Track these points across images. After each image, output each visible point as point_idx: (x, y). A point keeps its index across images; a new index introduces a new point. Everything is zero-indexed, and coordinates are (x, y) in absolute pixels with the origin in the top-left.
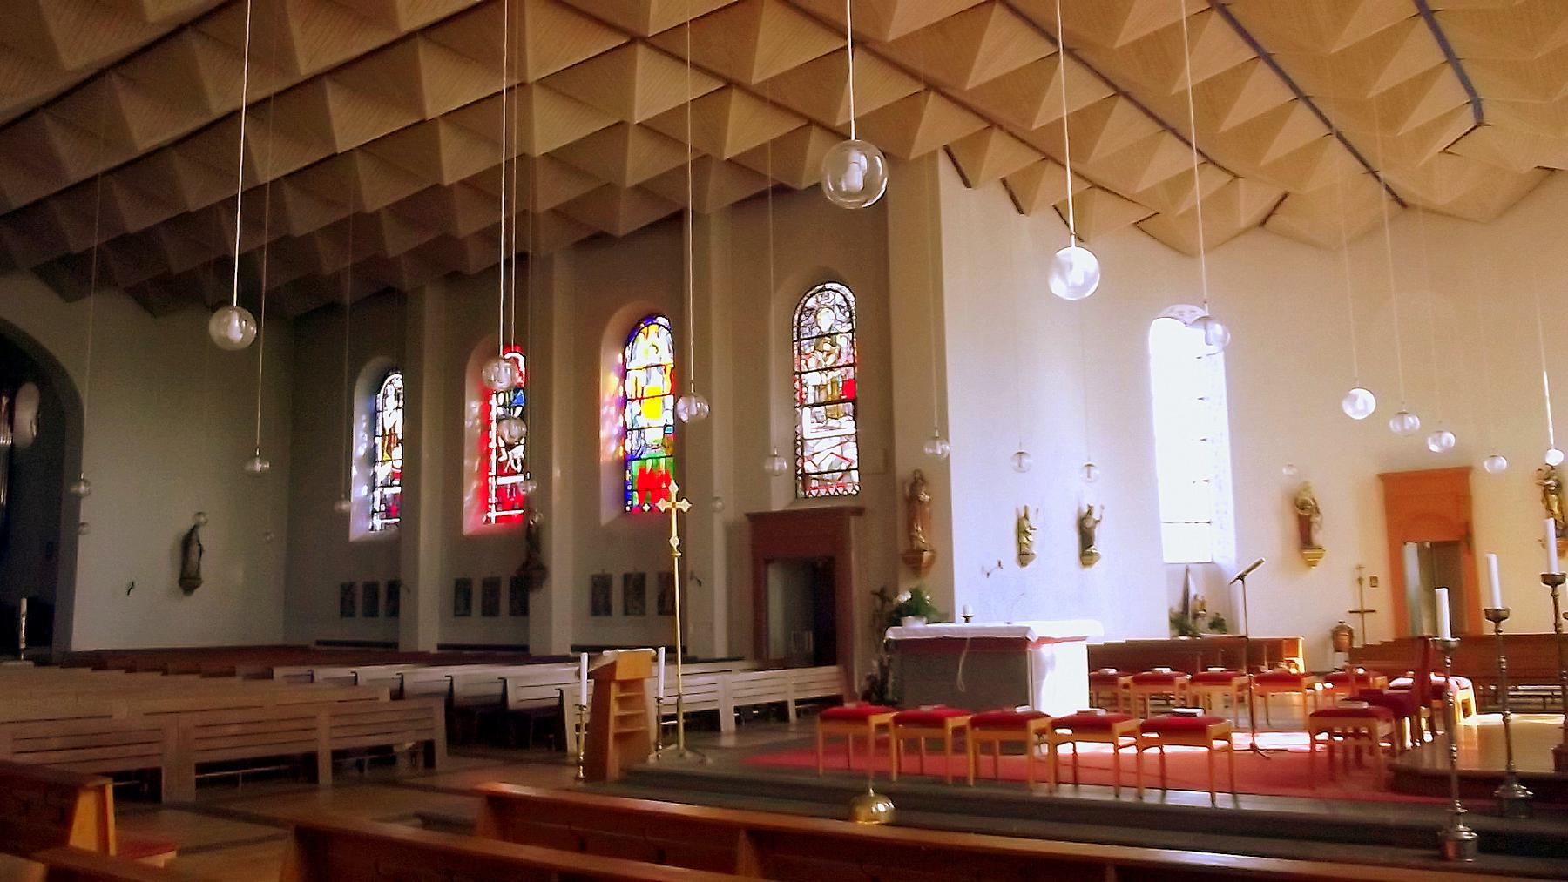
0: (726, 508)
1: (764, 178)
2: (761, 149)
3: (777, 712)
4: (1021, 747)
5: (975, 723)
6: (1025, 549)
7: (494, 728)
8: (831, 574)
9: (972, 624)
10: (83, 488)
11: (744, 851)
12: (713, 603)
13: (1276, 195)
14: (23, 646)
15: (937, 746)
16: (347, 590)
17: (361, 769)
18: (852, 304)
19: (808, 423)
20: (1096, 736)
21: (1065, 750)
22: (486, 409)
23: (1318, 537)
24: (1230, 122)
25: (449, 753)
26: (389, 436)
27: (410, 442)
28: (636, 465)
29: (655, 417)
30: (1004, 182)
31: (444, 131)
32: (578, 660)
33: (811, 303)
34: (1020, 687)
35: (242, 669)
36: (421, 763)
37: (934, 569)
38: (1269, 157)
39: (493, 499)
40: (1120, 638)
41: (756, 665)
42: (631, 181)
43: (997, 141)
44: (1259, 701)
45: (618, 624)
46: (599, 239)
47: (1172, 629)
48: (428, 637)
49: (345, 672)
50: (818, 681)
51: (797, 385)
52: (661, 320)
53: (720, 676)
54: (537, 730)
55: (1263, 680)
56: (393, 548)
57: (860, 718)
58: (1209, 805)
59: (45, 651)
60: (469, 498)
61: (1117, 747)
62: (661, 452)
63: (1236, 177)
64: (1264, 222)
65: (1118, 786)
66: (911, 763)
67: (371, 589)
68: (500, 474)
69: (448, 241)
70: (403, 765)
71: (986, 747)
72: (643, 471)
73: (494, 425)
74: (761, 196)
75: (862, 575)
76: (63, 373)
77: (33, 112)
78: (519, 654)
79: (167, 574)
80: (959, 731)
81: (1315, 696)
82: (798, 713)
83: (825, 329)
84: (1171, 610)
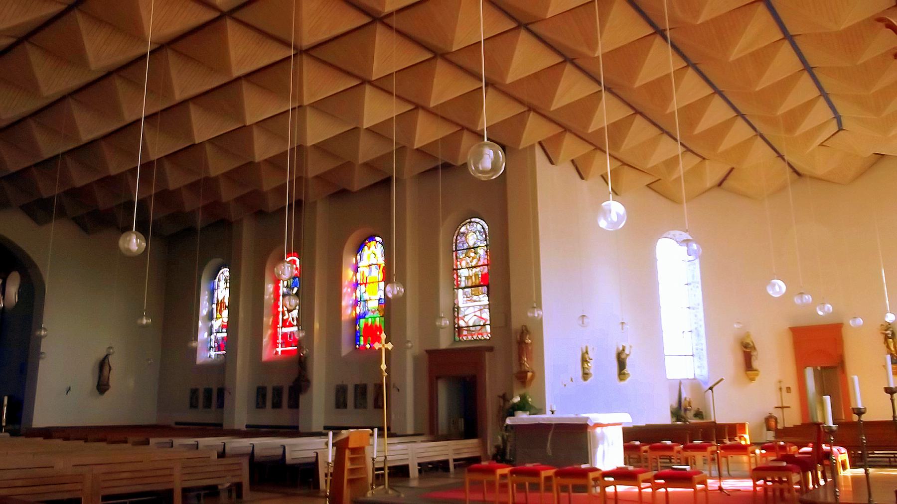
0: (414, 346)
1: (436, 159)
4: (584, 488)
5: (557, 474)
6: (586, 371)
8: (474, 387)
12: (407, 402)
14: (4, 424)
15: (535, 487)
16: (194, 392)
17: (199, 500)
18: (487, 231)
21: (610, 489)
22: (277, 288)
23: (755, 364)
26: (221, 304)
27: (233, 307)
30: (573, 161)
31: (256, 132)
33: (463, 229)
35: (131, 439)
36: (234, 495)
38: (722, 148)
39: (280, 341)
42: (360, 161)
45: (340, 418)
46: (342, 194)
49: (191, 441)
50: (466, 448)
51: (455, 276)
55: (726, 448)
56: (220, 368)
57: (491, 471)
60: (266, 339)
63: (704, 159)
64: (720, 185)
67: (208, 392)
68: (284, 325)
71: (564, 488)
72: (366, 325)
74: (435, 169)
78: (293, 431)
79: (89, 381)
80: (548, 479)
83: (471, 244)
84: (671, 406)
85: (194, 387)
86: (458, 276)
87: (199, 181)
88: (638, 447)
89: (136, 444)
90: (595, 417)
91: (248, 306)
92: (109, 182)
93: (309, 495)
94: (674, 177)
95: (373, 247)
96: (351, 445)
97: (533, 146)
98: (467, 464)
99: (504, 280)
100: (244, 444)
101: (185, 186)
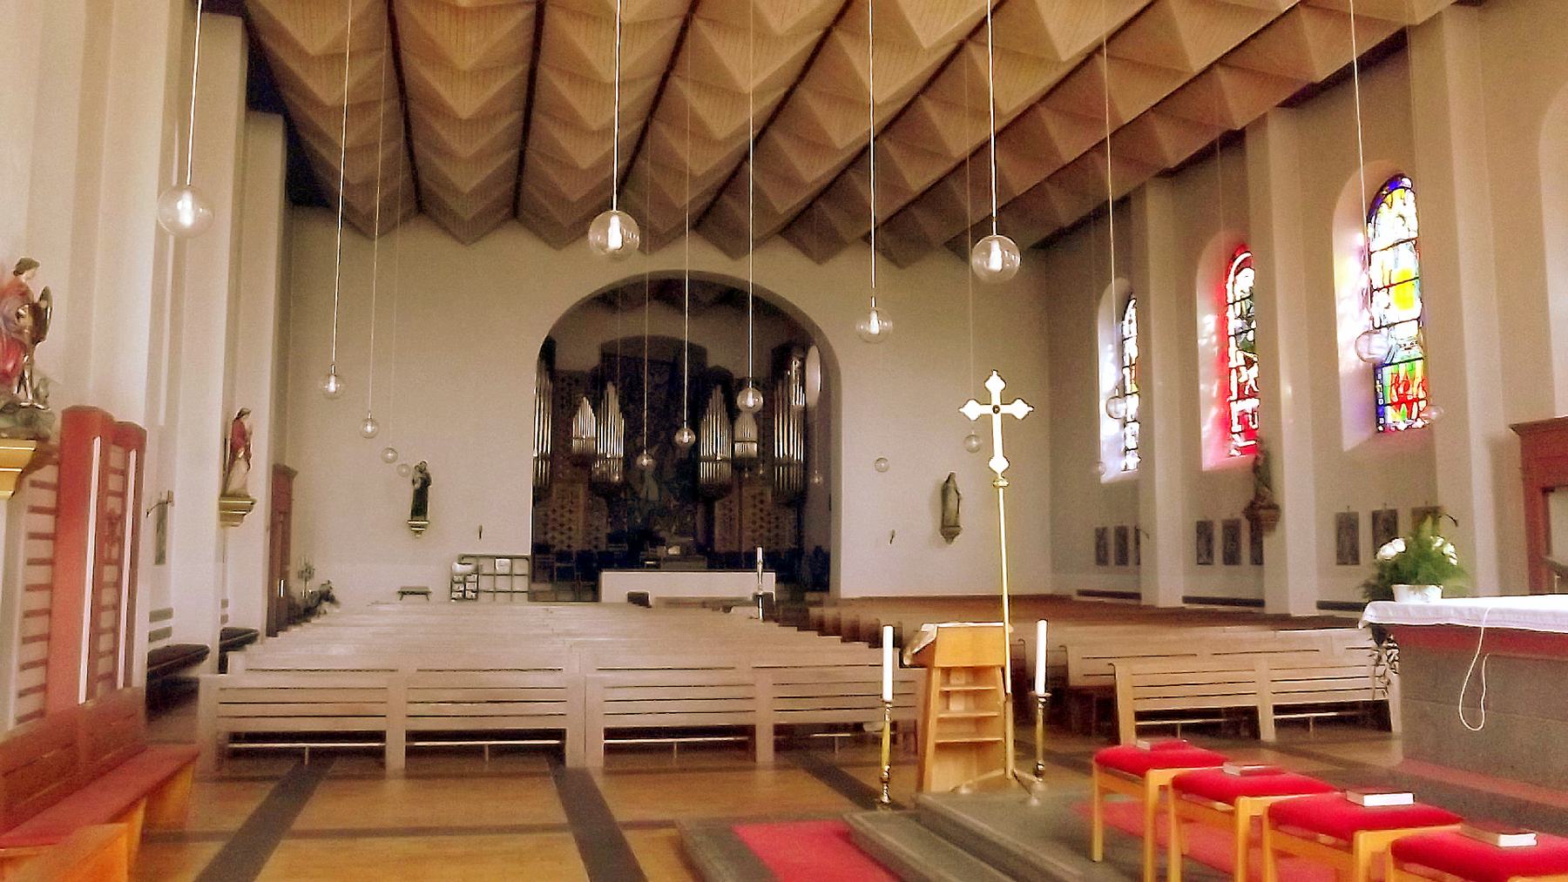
16: (1101, 534)
22: (1223, 321)
39: (1236, 428)
56: (1132, 490)
60: (1208, 427)
68: (1241, 397)
79: (929, 522)
82: (411, 753)
85: (1099, 526)
90: (142, 649)
91: (1168, 371)
92: (1075, 172)
95: (1397, 203)
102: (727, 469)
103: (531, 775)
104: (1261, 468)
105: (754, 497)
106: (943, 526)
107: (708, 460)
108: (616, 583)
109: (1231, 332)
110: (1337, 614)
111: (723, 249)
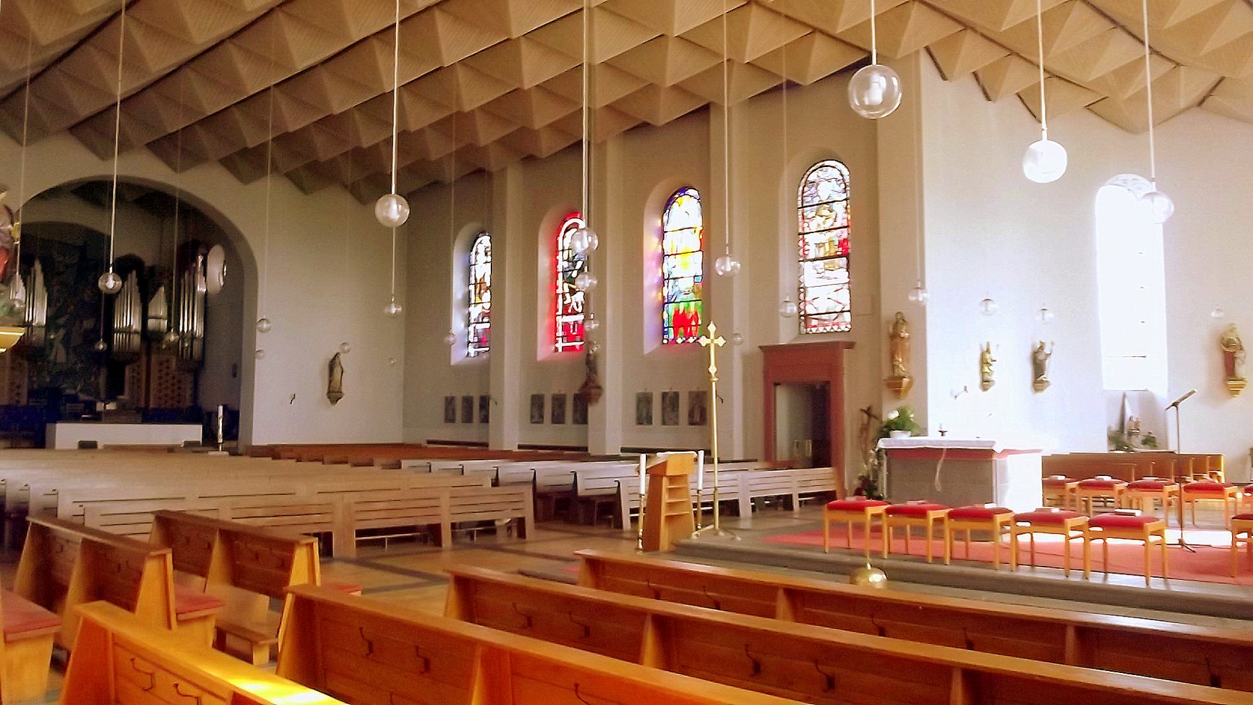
0: (747, 342)
1: (780, 77)
2: (776, 53)
3: (785, 502)
4: (987, 536)
5: (951, 515)
6: (987, 377)
7: (564, 508)
8: (822, 397)
9: (947, 437)
10: (452, 339)
11: (782, 604)
12: (732, 415)
13: (1214, 78)
14: (220, 441)
15: (920, 532)
16: (450, 401)
17: (472, 537)
18: (847, 179)
19: (810, 274)
20: (1046, 529)
21: (1024, 539)
23: (1241, 370)
24: (1173, 20)
25: (537, 528)
26: (479, 284)
27: (496, 288)
28: (671, 308)
29: (686, 268)
30: (975, 75)
31: (525, 47)
32: (637, 459)
33: (812, 177)
34: (986, 489)
35: (379, 461)
36: (515, 534)
37: (911, 392)
38: (1208, 48)
39: (560, 333)
40: (1065, 451)
41: (766, 465)
42: (669, 83)
43: (969, 40)
44: (1186, 505)
45: (655, 434)
46: (643, 128)
47: (1109, 444)
48: (511, 442)
49: (455, 464)
50: (819, 479)
51: (801, 243)
52: (691, 192)
53: (740, 473)
54: (602, 511)
55: (1189, 488)
56: (483, 371)
57: (860, 508)
58: (1144, 586)
59: (233, 444)
61: (1068, 538)
62: (691, 296)
63: (1178, 64)
64: (1201, 103)
65: (1068, 569)
66: (898, 545)
67: (468, 401)
68: (565, 313)
69: (526, 132)
70: (501, 537)
71: (960, 535)
72: (677, 312)
73: (560, 275)
74: (778, 88)
75: (852, 399)
76: (240, 237)
77: (222, 42)
78: (581, 453)
79: (321, 387)
80: (938, 521)
81: (1236, 504)
84: (1109, 428)
86: (805, 244)
87: (451, 116)
88: (1062, 484)
89: (385, 467)
93: (609, 536)
94: (1131, 92)
96: (670, 472)
97: (917, 52)
98: (823, 498)
99: (869, 249)
100: (524, 469)
101: (430, 126)
102: (136, 340)
103: (405, 554)
104: (591, 365)
105: (161, 364)
106: (329, 392)
107: (120, 331)
108: (67, 434)
109: (560, 269)
110: (631, 454)
111: (93, 149)
